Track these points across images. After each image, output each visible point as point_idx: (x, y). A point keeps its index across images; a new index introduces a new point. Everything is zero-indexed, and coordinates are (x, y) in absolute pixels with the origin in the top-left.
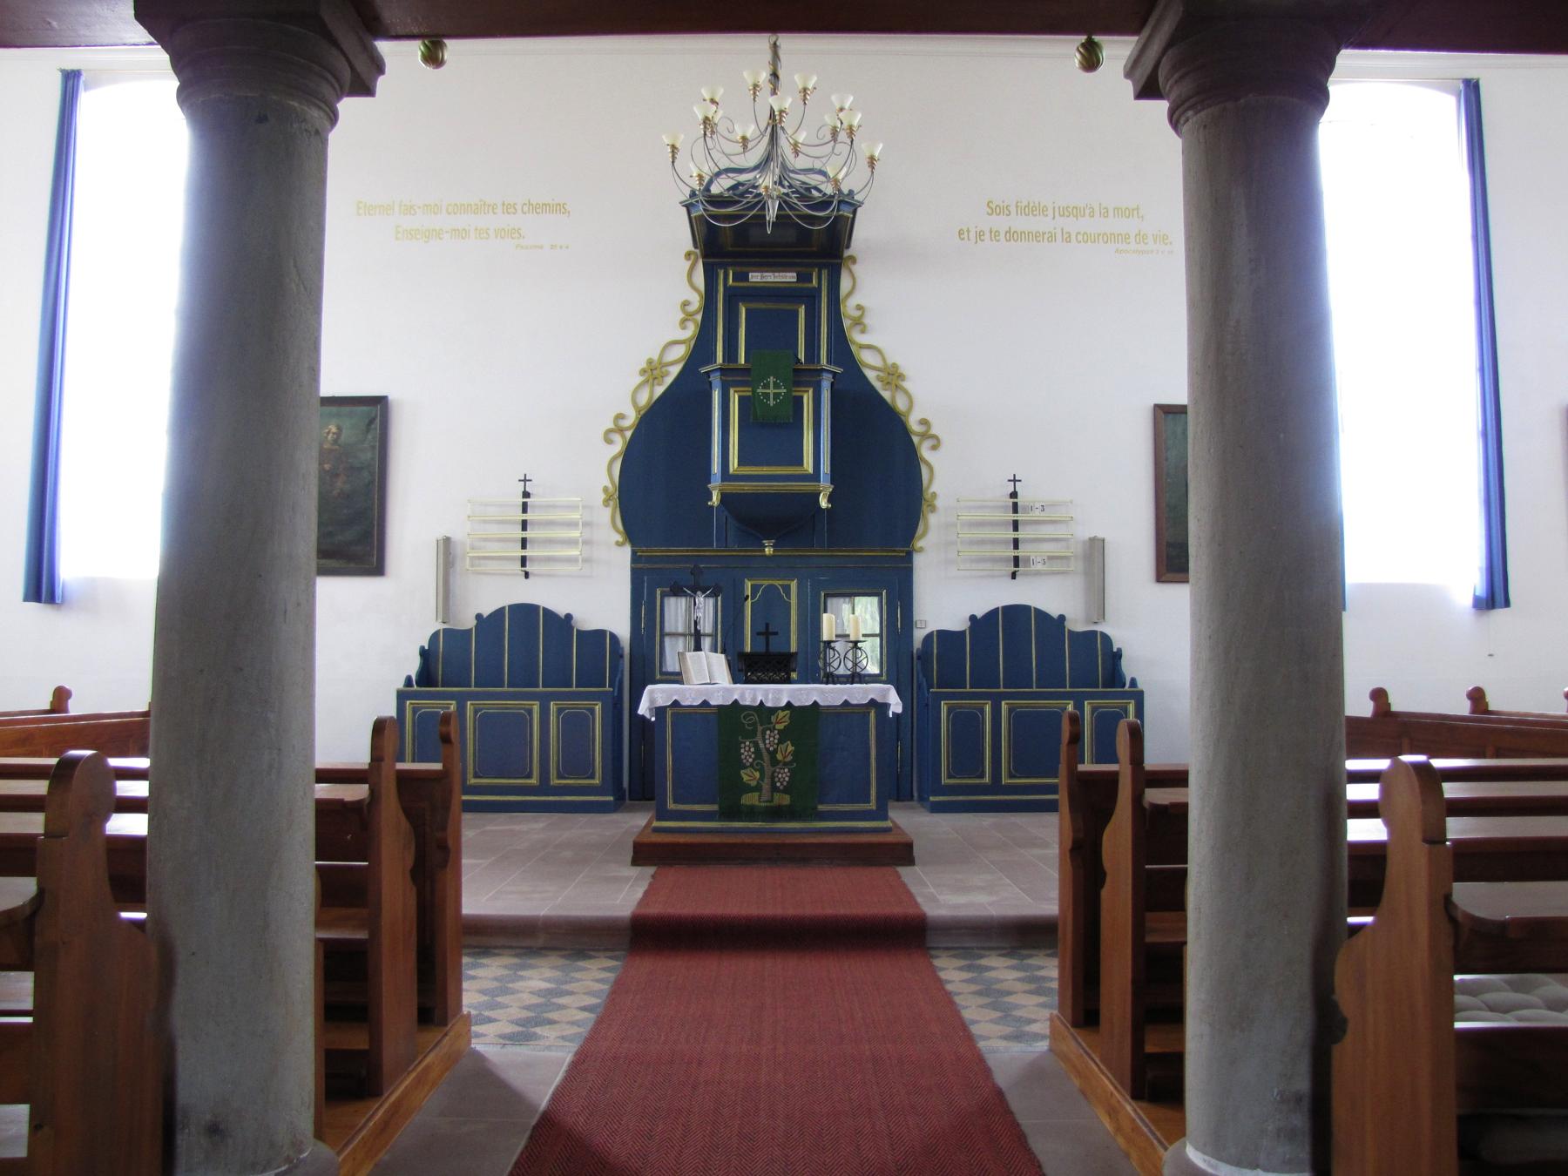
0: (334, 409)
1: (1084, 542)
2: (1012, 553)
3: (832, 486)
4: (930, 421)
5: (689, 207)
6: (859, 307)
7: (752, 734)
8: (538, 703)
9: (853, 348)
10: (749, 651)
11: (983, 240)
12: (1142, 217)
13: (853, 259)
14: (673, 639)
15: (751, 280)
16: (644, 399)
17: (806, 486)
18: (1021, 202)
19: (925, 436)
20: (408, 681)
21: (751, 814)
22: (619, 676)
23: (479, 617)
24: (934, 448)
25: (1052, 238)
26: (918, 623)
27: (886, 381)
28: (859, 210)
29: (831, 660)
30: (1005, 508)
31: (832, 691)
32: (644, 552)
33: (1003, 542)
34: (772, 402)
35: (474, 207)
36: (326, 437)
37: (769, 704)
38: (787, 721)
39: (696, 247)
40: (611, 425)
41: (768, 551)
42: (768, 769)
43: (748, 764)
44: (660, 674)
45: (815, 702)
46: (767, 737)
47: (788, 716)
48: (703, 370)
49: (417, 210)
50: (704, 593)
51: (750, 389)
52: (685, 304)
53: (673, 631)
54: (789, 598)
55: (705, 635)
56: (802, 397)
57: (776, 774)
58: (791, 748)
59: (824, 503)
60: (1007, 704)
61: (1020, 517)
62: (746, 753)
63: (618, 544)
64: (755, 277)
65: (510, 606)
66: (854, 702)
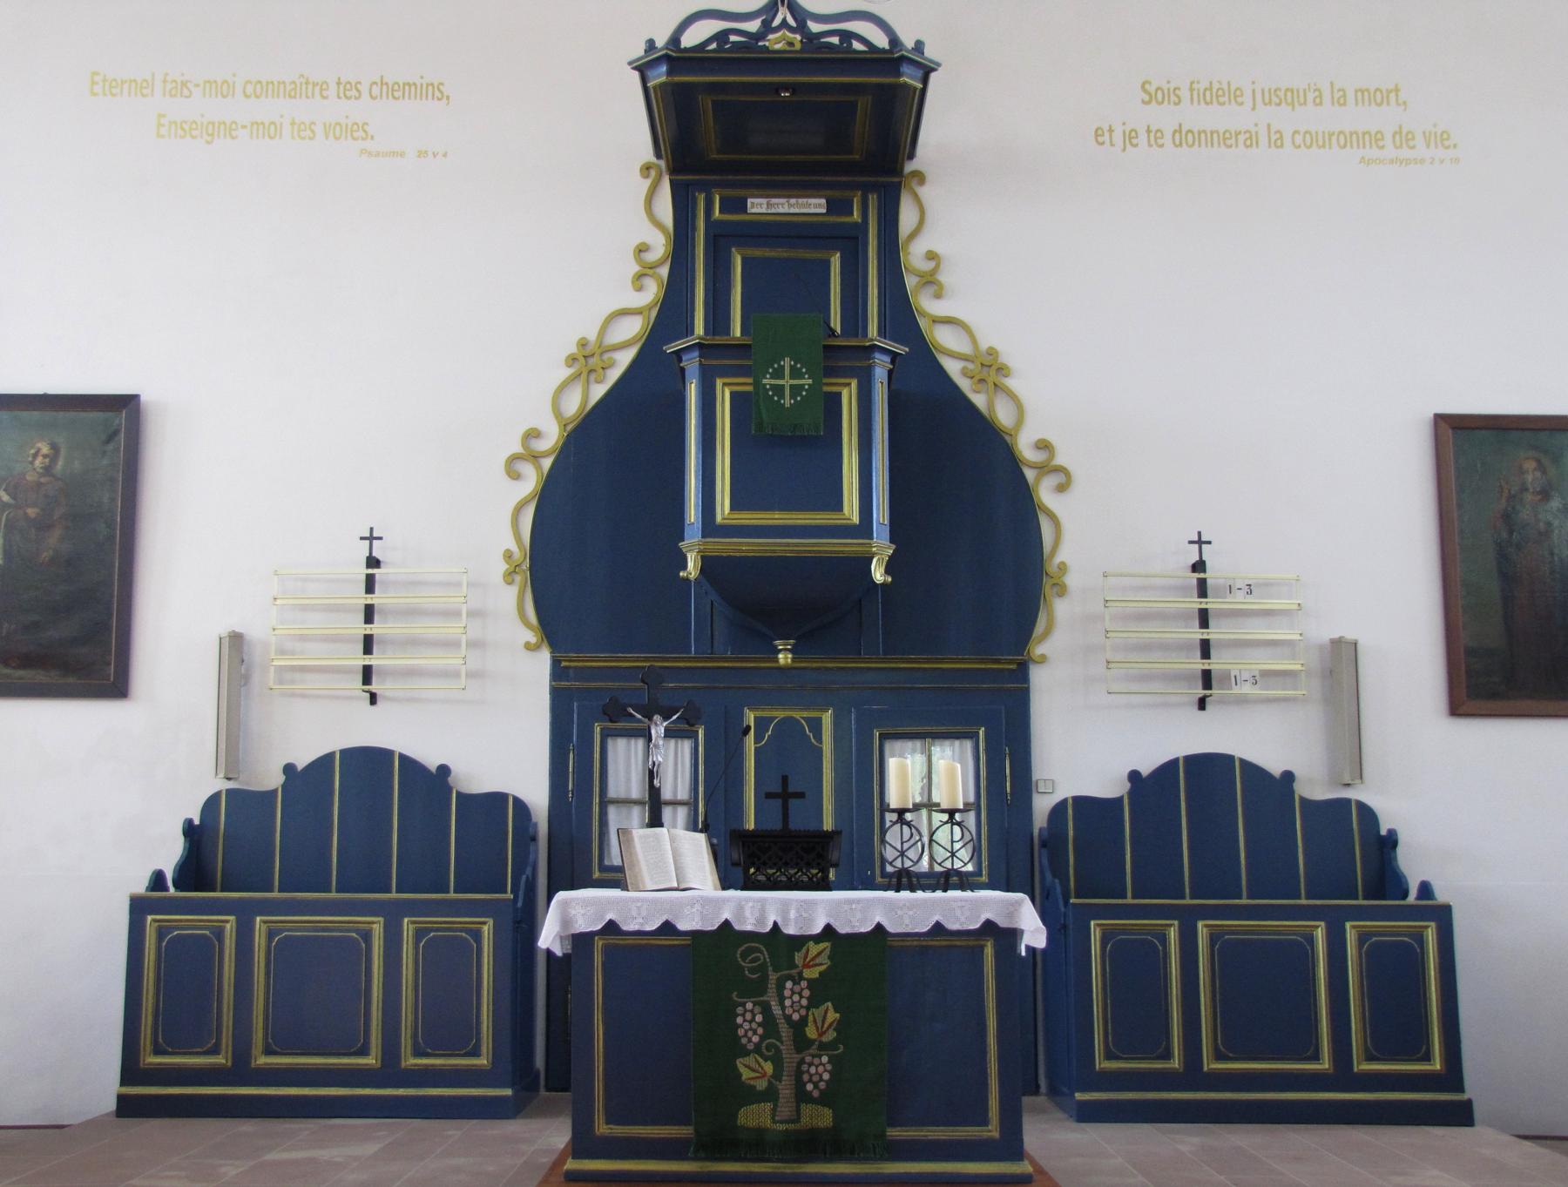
0: (48, 415)
1: (1321, 647)
2: (1199, 665)
3: (894, 547)
4: (1054, 443)
5: (643, 69)
6: (931, 256)
7: (756, 989)
8: (381, 919)
9: (922, 323)
10: (752, 827)
11: (1136, 145)
12: (1405, 103)
13: (920, 177)
14: (624, 810)
15: (750, 210)
16: (573, 405)
17: (847, 546)
18: (1198, 82)
19: (1046, 469)
20: (158, 880)
21: (757, 1145)
22: (529, 871)
23: (289, 769)
24: (1062, 488)
25: (1251, 140)
26: (1041, 784)
27: (978, 377)
28: (933, 76)
29: (906, 846)
30: (1183, 590)
31: (913, 905)
32: (571, 662)
33: (1183, 647)
34: (787, 401)
35: (289, 88)
36: (32, 463)
37: (790, 930)
38: (825, 963)
39: (658, 155)
40: (517, 448)
41: (784, 658)
42: (789, 1056)
43: (750, 1047)
44: (600, 871)
45: (879, 927)
46: (787, 993)
47: (828, 952)
48: (670, 349)
49: (193, 89)
50: (666, 718)
51: (750, 380)
52: (642, 249)
53: (622, 795)
54: (820, 740)
55: (675, 803)
56: (839, 395)
57: (805, 1068)
58: (832, 1016)
59: (878, 574)
60: (1206, 926)
61: (1211, 603)
62: (747, 1026)
63: (528, 647)
64: (758, 206)
65: (344, 752)
66: (953, 926)
